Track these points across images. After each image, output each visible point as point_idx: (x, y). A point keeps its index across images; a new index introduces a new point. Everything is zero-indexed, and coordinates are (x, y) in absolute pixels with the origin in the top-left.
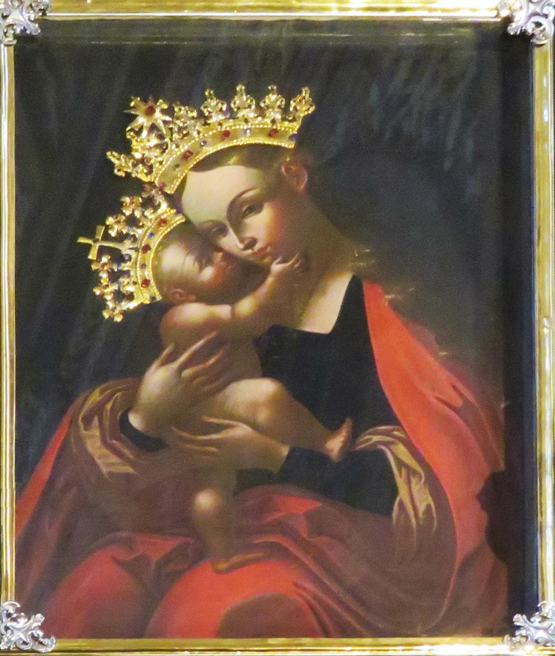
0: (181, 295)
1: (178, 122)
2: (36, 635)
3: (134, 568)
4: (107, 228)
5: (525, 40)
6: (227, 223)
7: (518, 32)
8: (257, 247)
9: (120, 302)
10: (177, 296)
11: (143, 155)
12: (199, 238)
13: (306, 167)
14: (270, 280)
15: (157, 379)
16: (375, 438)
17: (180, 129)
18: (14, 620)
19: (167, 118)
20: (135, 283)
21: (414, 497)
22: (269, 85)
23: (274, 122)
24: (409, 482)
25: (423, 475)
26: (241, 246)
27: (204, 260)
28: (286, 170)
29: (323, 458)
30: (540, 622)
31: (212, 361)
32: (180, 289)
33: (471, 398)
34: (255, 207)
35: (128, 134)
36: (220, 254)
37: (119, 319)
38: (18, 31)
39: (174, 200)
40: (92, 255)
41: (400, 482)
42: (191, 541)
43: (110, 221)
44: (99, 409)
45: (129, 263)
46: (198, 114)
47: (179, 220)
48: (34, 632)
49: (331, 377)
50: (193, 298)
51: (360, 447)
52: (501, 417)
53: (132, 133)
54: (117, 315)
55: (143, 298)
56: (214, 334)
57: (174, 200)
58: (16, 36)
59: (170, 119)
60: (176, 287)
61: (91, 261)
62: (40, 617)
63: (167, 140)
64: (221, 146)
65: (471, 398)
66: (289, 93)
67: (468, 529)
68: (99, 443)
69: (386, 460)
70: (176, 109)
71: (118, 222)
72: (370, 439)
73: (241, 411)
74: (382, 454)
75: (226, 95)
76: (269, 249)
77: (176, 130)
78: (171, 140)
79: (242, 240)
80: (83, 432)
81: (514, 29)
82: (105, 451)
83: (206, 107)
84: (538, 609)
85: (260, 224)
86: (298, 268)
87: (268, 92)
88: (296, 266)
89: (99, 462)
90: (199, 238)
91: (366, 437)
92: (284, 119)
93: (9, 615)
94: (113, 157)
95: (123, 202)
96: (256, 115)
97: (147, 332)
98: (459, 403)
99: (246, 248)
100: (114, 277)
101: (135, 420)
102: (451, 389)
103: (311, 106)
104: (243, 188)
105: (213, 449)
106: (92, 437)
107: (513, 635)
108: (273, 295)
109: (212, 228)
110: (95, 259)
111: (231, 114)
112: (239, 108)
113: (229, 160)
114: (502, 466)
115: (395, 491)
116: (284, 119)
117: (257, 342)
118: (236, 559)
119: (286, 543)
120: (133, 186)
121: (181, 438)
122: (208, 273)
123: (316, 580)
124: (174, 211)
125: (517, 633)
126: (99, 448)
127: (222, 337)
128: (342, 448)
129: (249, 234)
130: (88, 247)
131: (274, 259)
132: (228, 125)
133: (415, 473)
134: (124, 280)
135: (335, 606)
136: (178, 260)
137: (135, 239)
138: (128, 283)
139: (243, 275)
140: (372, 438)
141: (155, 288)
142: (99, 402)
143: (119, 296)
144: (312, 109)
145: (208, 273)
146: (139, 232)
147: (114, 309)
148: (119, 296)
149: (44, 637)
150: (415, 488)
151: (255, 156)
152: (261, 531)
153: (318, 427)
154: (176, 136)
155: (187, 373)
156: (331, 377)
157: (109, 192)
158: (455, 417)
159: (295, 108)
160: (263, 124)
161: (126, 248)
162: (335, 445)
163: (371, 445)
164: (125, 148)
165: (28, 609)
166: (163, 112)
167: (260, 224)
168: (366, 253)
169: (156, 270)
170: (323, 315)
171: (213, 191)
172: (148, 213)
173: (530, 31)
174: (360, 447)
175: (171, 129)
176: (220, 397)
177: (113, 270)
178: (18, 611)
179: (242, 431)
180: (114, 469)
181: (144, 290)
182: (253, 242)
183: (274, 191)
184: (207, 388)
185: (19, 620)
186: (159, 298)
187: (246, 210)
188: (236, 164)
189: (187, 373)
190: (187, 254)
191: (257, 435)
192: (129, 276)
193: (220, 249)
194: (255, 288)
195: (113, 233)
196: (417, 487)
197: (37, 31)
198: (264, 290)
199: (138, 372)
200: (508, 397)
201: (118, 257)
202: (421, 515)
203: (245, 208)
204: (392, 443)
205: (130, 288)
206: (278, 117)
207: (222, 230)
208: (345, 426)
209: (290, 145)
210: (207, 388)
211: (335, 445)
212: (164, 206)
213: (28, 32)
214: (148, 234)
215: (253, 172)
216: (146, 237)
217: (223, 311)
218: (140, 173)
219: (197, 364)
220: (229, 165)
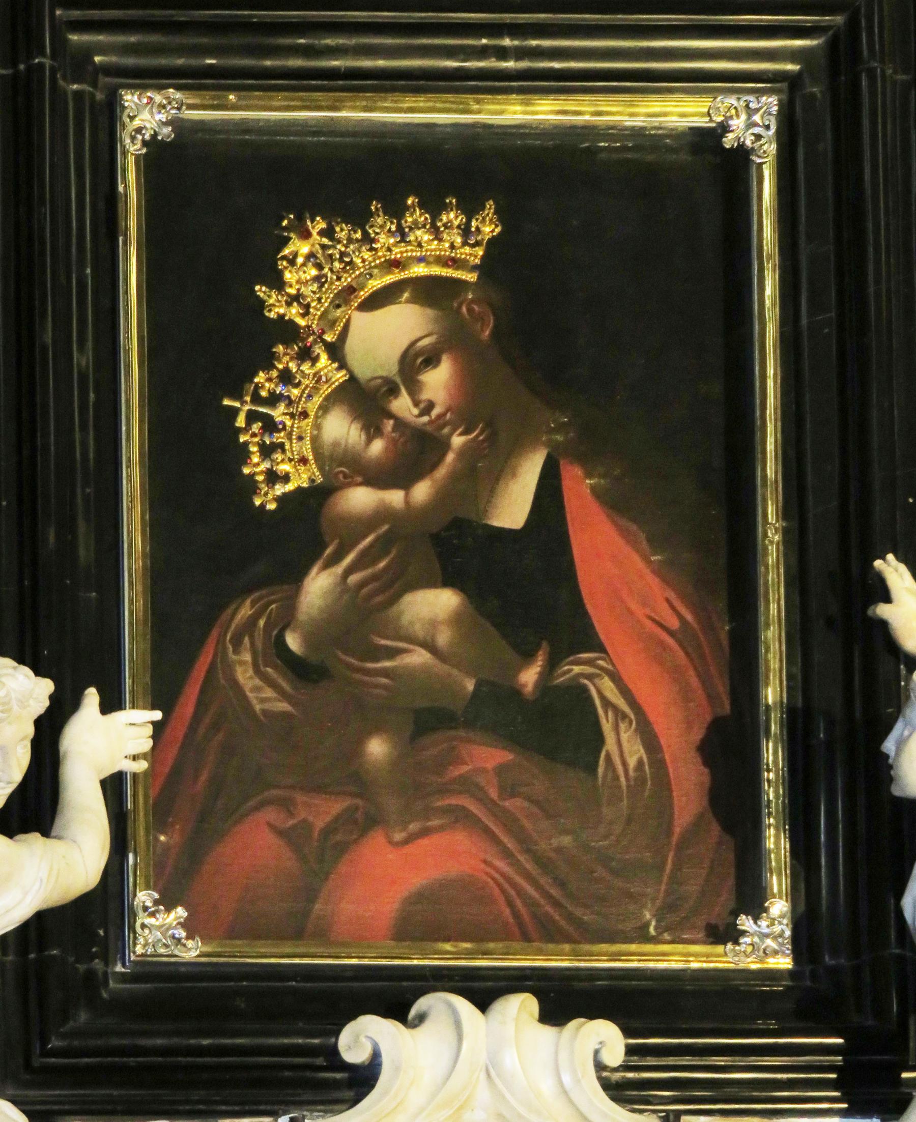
0: (345, 476)
1: (339, 246)
2: (177, 936)
3: (294, 837)
4: (257, 387)
5: (742, 154)
6: (398, 380)
7: (736, 145)
8: (435, 412)
9: (274, 484)
10: (341, 476)
11: (299, 290)
12: (365, 400)
13: (490, 305)
14: (450, 457)
15: (318, 587)
16: (577, 669)
17: (342, 254)
18: (153, 915)
19: (325, 241)
20: (290, 460)
21: (623, 747)
22: (447, 197)
23: (452, 247)
24: (616, 728)
25: (632, 717)
26: (416, 411)
27: (372, 430)
28: (469, 310)
29: (516, 693)
30: (768, 926)
31: (382, 564)
32: (344, 468)
33: (689, 617)
34: (431, 360)
35: (279, 263)
36: (391, 422)
37: (272, 506)
38: (147, 137)
39: (336, 352)
40: (241, 422)
41: (607, 727)
42: (359, 802)
43: (260, 378)
44: (252, 622)
45: (282, 434)
46: (362, 234)
47: (340, 377)
48: (176, 932)
49: (523, 588)
50: (359, 479)
51: (558, 681)
52: (725, 643)
53: (285, 263)
54: (270, 501)
55: (300, 479)
56: (386, 527)
57: (336, 352)
58: (145, 143)
59: (330, 243)
60: (340, 466)
61: (239, 431)
62: (181, 912)
63: (326, 270)
64: (389, 279)
65: (689, 617)
66: (470, 209)
67: (689, 782)
68: (251, 672)
69: (589, 698)
70: (338, 229)
71: (270, 380)
72: (572, 670)
73: (419, 630)
74: (585, 689)
75: (396, 211)
76: (448, 415)
77: (338, 256)
78: (331, 270)
79: (416, 404)
80: (233, 657)
81: (729, 141)
82: (257, 682)
83: (371, 227)
84: (766, 910)
85: (438, 381)
86: (483, 441)
87: (446, 208)
88: (481, 438)
89: (250, 695)
90: (365, 400)
91: (566, 668)
92: (465, 243)
93: (145, 909)
94: (260, 290)
95: (275, 352)
96: (431, 238)
97: (306, 526)
98: (674, 624)
99: (421, 414)
100: (267, 451)
101: (293, 642)
102: (666, 605)
103: (497, 226)
104: (419, 334)
105: (384, 681)
106: (242, 663)
107: (736, 942)
108: (454, 477)
109: (381, 386)
110: (244, 426)
111: (402, 234)
112: (411, 229)
113: (401, 296)
114: (727, 709)
115: (599, 739)
116: (465, 243)
117: (437, 539)
118: (413, 827)
119: (474, 808)
120: (287, 331)
121: (349, 666)
122: (377, 447)
123: (507, 854)
124: (336, 365)
125: (742, 940)
126: (251, 678)
127: (394, 530)
128: (537, 684)
129: (425, 395)
130: (235, 412)
131: (454, 430)
132: (397, 252)
133: (624, 716)
134: (278, 456)
135: (531, 890)
136: (340, 428)
137: (290, 402)
138: (283, 461)
139: (416, 452)
140: (573, 670)
141: (314, 466)
142: (250, 616)
143: (273, 477)
144: (498, 230)
145: (377, 447)
146: (295, 392)
147: (266, 494)
148: (273, 477)
149: (187, 938)
150: (624, 736)
151: (429, 292)
152: (444, 790)
153: (509, 654)
154: (337, 265)
155: (354, 579)
156: (523, 588)
157: (258, 341)
158: (670, 641)
159: (478, 229)
160: (440, 250)
161: (278, 413)
162: (529, 677)
163: (570, 679)
164: (278, 283)
165: (167, 902)
166: (322, 233)
167: (438, 381)
168: (564, 423)
169: (316, 441)
170: (513, 506)
171: (384, 335)
172: (306, 367)
173: (748, 143)
174: (558, 681)
175: (331, 256)
176: (395, 609)
177: (264, 442)
178: (156, 902)
179: (418, 657)
180: (267, 706)
181: (302, 468)
182: (431, 405)
183: (453, 340)
184: (379, 599)
185: (158, 916)
186: (319, 480)
187: (421, 363)
188: (407, 301)
189: (354, 579)
190: (354, 419)
191: (437, 662)
192: (284, 451)
193: (390, 415)
194: (435, 466)
195: (264, 394)
196: (628, 734)
197: (169, 136)
198: (441, 472)
199: (295, 576)
200: (732, 618)
201: (270, 426)
202: (631, 773)
203: (420, 360)
204: (598, 675)
205: (285, 467)
206: (458, 240)
207: (393, 391)
208: (541, 653)
209: (472, 277)
210: (379, 599)
211: (529, 677)
212: (324, 360)
213: (160, 138)
214: (305, 395)
215: (430, 312)
216: (303, 399)
217: (395, 497)
218: (294, 312)
219: (365, 567)
220: (400, 303)
